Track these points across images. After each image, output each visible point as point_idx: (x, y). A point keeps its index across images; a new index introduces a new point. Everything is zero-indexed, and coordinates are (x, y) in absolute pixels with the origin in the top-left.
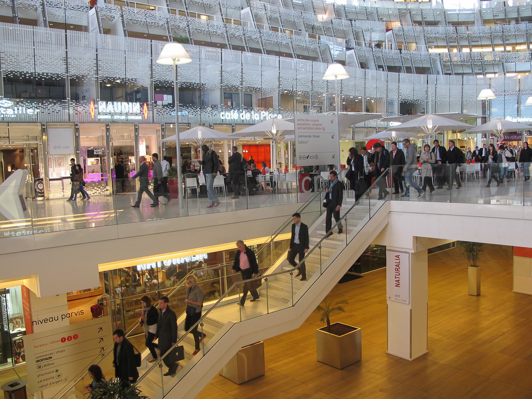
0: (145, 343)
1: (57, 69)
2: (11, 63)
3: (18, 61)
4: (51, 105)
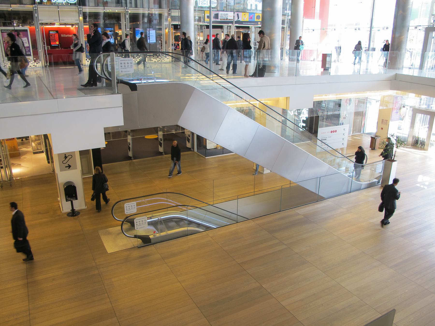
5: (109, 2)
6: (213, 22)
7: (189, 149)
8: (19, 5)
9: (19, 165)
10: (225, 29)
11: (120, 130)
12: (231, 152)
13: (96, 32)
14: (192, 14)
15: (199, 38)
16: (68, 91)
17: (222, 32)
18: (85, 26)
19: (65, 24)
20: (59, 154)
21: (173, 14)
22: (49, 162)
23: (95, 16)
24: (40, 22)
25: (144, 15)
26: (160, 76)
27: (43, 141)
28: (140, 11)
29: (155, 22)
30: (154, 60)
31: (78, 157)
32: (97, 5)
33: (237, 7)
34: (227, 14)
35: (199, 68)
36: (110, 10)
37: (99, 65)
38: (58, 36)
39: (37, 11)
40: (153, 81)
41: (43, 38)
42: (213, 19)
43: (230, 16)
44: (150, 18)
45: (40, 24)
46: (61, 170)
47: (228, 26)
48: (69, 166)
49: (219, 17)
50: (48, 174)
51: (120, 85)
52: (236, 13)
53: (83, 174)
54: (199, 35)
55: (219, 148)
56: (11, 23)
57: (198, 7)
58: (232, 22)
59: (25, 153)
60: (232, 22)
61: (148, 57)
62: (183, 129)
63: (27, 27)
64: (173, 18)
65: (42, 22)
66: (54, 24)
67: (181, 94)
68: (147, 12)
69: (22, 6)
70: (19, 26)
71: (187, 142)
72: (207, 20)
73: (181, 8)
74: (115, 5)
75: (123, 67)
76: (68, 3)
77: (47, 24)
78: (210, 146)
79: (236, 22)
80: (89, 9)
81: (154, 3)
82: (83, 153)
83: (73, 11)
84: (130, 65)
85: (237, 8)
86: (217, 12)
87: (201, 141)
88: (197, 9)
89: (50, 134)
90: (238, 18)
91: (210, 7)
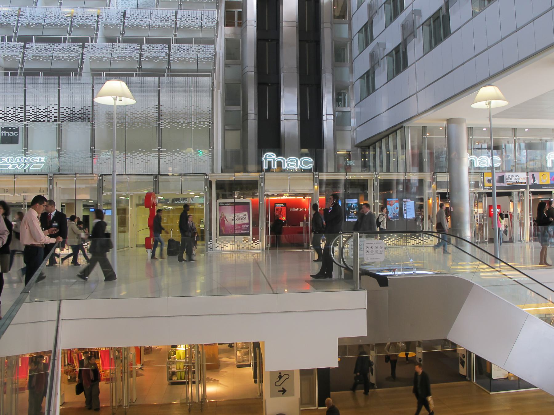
0: (5, 282)
1: (149, 118)
2: (33, 113)
3: (40, 111)
4: (140, 155)
5: (354, 166)
6: (498, 188)
7: (463, 378)
8: (243, 174)
9: (216, 382)
10: (514, 197)
11: (361, 342)
12: (533, 387)
13: (336, 205)
14: (466, 178)
15: (476, 210)
16: (293, 284)
17: (511, 201)
18: (320, 198)
19: (296, 195)
20: (271, 372)
21: (439, 179)
22: (256, 382)
23: (334, 184)
24: (266, 193)
25: (398, 180)
26: (420, 265)
27: (252, 350)
28: (394, 176)
29: (414, 190)
30: (412, 242)
31: (297, 378)
32: (337, 170)
33: (531, 165)
34: (516, 176)
35: (478, 253)
36: (353, 176)
37: (337, 248)
38: (285, 210)
39: (263, 180)
40: (412, 272)
41: (267, 213)
42: (496, 184)
43: (522, 177)
44: (407, 183)
45: (265, 195)
46: (272, 396)
47: (519, 192)
48: (284, 391)
49: (506, 181)
50: (252, 399)
51: (365, 277)
52: (530, 174)
53: (302, 403)
54: (476, 206)
55: (512, 378)
56: (231, 195)
57: (474, 168)
58: (525, 187)
59: (227, 365)
60: (525, 187)
61: (403, 237)
62: (454, 345)
63: (249, 200)
64: (440, 185)
65: (268, 193)
66: (282, 195)
67: (452, 293)
68: (402, 177)
69: (247, 174)
70: (239, 198)
71: (460, 366)
72: (487, 184)
73: (449, 171)
74: (360, 169)
75: (370, 253)
76: (301, 169)
77: (273, 195)
78: (497, 374)
79: (531, 187)
80: (327, 175)
81: (413, 165)
82: (305, 373)
83: (306, 179)
84: (379, 249)
85: (531, 167)
86: (502, 174)
87: (483, 367)
88: (472, 171)
89: (263, 342)
90: (534, 180)
91: (492, 168)
